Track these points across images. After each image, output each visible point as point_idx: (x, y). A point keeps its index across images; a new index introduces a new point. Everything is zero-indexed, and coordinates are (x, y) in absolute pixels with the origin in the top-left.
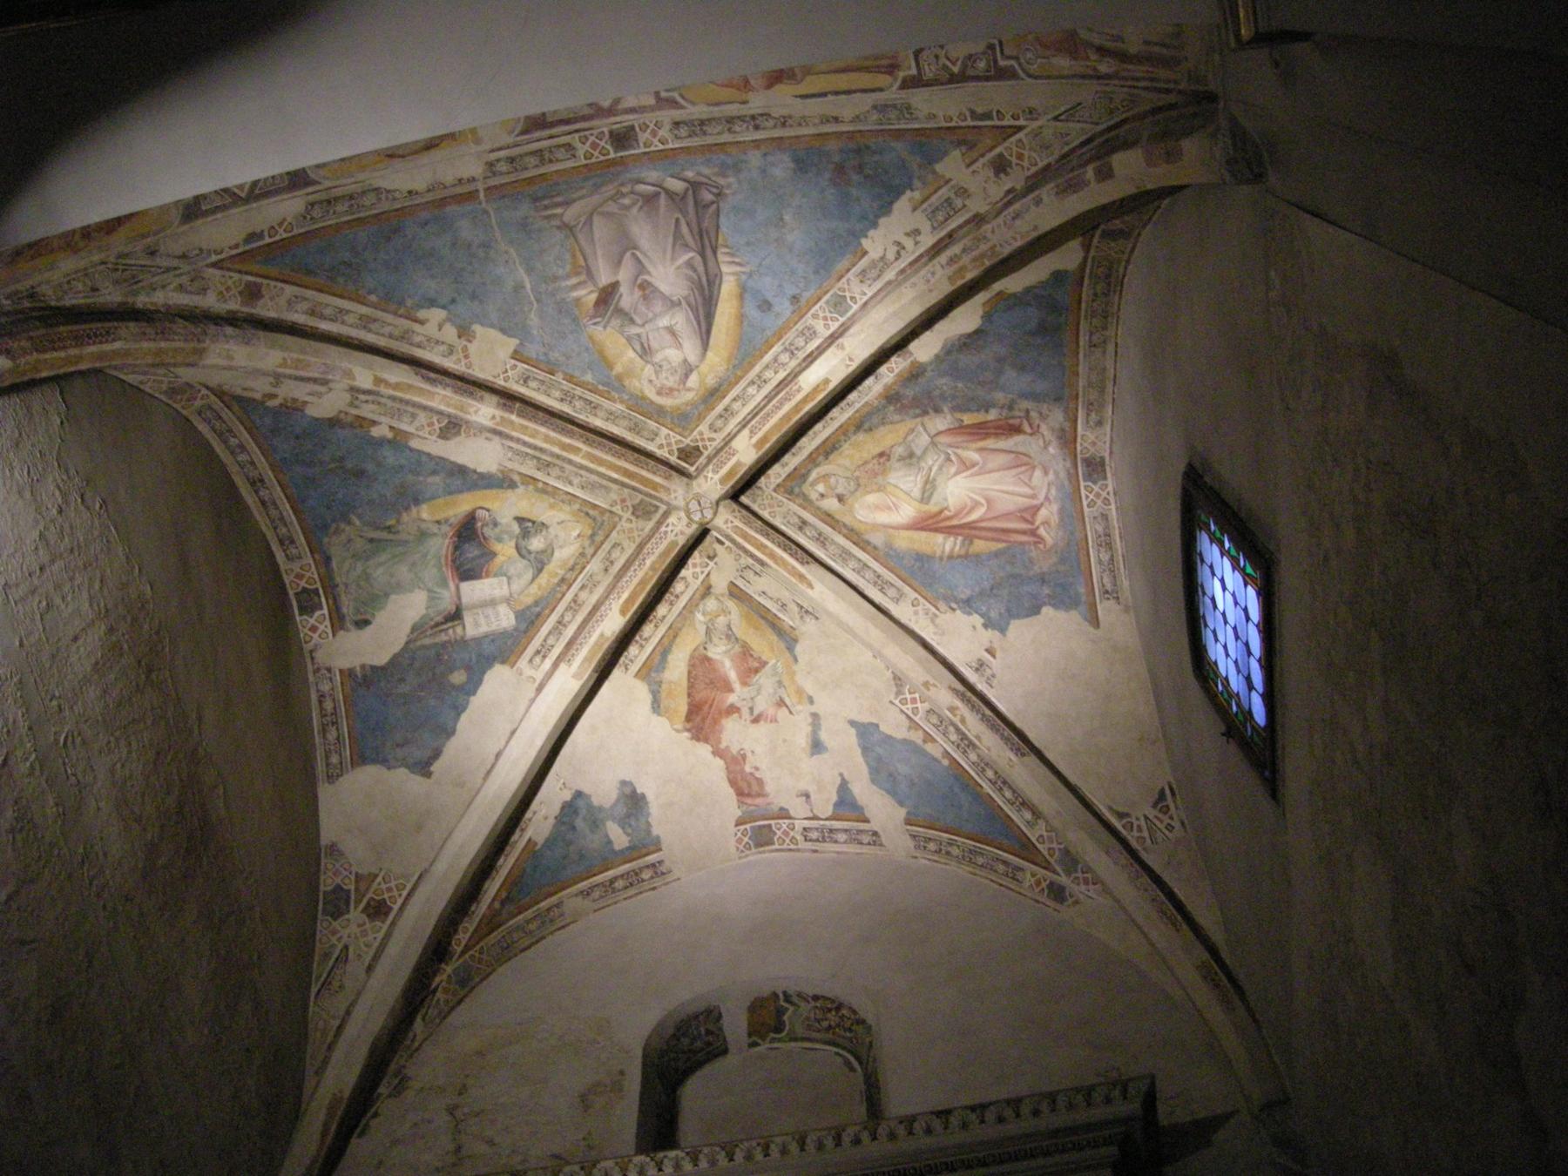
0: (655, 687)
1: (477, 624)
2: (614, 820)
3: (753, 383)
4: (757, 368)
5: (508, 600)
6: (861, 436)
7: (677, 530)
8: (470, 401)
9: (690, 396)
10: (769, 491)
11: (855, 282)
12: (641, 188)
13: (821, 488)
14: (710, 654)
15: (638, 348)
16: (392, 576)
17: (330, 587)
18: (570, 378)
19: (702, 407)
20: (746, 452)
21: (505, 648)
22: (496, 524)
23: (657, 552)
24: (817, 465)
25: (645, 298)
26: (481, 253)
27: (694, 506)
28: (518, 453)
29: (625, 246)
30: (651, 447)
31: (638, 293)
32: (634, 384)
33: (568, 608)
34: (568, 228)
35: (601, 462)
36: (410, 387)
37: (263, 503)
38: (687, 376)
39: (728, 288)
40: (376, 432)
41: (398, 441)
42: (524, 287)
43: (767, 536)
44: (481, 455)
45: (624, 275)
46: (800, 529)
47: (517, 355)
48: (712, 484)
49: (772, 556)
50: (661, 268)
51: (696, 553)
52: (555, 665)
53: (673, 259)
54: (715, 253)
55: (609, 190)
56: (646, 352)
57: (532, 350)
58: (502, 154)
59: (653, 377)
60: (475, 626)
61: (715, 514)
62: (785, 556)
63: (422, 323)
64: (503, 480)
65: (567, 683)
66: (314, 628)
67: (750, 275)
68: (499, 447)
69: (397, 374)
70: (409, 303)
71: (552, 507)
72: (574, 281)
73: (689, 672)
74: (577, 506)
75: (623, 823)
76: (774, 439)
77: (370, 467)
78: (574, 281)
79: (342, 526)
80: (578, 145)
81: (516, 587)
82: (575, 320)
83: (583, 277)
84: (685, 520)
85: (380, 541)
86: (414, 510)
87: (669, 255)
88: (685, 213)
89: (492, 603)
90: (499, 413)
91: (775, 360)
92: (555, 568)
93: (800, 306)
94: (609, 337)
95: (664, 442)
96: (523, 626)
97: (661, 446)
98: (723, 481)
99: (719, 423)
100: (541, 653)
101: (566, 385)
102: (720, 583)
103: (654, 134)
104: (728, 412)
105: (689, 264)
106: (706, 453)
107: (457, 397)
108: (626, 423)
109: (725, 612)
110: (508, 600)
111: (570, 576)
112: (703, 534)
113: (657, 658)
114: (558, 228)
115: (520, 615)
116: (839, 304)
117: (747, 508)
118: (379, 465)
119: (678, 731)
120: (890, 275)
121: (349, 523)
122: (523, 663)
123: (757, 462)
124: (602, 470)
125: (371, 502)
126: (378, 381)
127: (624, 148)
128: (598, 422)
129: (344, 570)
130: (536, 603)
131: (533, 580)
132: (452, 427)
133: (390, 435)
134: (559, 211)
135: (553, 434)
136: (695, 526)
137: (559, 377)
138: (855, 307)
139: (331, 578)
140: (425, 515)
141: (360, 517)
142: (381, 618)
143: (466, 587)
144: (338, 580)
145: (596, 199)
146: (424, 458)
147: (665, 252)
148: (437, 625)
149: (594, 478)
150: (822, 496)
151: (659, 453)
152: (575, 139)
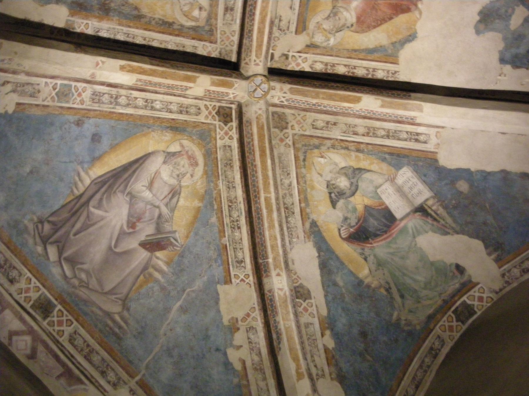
0: (397, 45)
1: (420, 193)
2: (507, 26)
3: (153, 108)
4: (141, 112)
5: (392, 180)
6: (145, 11)
7: (281, 94)
8: (277, 299)
9: (186, 142)
10: (218, 46)
11: (42, 96)
12: (68, 273)
13: (196, 13)
14: (354, 20)
15: (175, 200)
16: (417, 268)
17: (446, 305)
18: (222, 232)
19: (189, 129)
20: (203, 83)
21: (426, 165)
22: (346, 219)
23: (304, 99)
24: (182, 26)
25: (139, 219)
26: (175, 353)
27: (259, 93)
28: (291, 235)
29: (114, 256)
30: (235, 144)
31: (139, 226)
32: (201, 186)
33: (375, 136)
34: (125, 302)
35: (266, 177)
36: (291, 349)
37: (417, 387)
38: (174, 154)
39: (99, 171)
40: (331, 344)
41: (329, 324)
42: (181, 306)
43: (251, 31)
44: (305, 259)
45: (132, 243)
46: (232, 9)
47: (228, 281)
48: (237, 90)
49: (262, 21)
50: (113, 223)
51: (289, 68)
52: (419, 125)
53: (103, 218)
54: (81, 196)
55: (83, 293)
56: (175, 193)
57: (218, 271)
58: (103, 382)
59: (188, 175)
60: (422, 194)
61: (255, 75)
62: (258, 12)
63: (244, 362)
64: (313, 233)
65: (430, 114)
66: (479, 300)
67: (81, 163)
68: (293, 251)
69: (289, 366)
70: (236, 380)
71: (313, 188)
72: (157, 275)
73: (375, 27)
74: (303, 170)
75: (507, 17)
76: (182, 73)
77: (355, 331)
78: (157, 275)
79: (403, 322)
80: (66, 334)
81: (379, 180)
82: (182, 256)
83: (151, 270)
84: (272, 92)
85: (399, 290)
86: (366, 281)
87: (102, 223)
88: (67, 233)
89: (400, 190)
90: (273, 273)
91: (128, 105)
92: (353, 160)
93: (82, 117)
94: (179, 225)
95: (226, 138)
96: (405, 160)
97: (231, 138)
98: (230, 86)
99: (193, 110)
100: (415, 137)
101: (228, 231)
102: (302, 40)
103: (28, 290)
104: (183, 110)
105: (99, 206)
106: (218, 104)
107: (279, 310)
108: (229, 173)
109: (319, 25)
110: (392, 180)
111: (352, 147)
112: (275, 73)
113: (376, 55)
114: (128, 310)
115: (398, 167)
116: (64, 94)
117: (239, 53)
118: (351, 326)
119: (421, 13)
120: (22, 78)
121: (399, 319)
122: (430, 147)
123: (203, 72)
124: (270, 173)
125: (378, 314)
126: (300, 376)
127: (49, 302)
128: (240, 192)
129: (431, 301)
130: (384, 160)
131: (369, 171)
132: (300, 293)
133: (328, 332)
134: (117, 318)
135: (266, 225)
136: (272, 84)
137: (225, 240)
138: (59, 82)
139: (441, 307)
140: (366, 271)
141: (392, 315)
142: (450, 259)
143: (398, 215)
144: (440, 302)
145: (94, 297)
146: (330, 298)
147: (101, 227)
148: (435, 219)
149: (278, 171)
150: (201, 9)
151: (236, 136)
152: (64, 340)
